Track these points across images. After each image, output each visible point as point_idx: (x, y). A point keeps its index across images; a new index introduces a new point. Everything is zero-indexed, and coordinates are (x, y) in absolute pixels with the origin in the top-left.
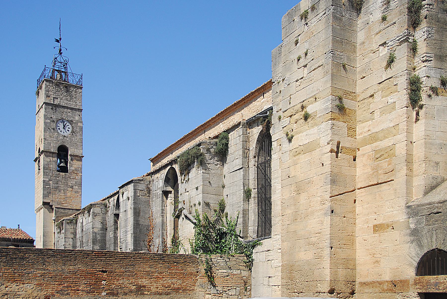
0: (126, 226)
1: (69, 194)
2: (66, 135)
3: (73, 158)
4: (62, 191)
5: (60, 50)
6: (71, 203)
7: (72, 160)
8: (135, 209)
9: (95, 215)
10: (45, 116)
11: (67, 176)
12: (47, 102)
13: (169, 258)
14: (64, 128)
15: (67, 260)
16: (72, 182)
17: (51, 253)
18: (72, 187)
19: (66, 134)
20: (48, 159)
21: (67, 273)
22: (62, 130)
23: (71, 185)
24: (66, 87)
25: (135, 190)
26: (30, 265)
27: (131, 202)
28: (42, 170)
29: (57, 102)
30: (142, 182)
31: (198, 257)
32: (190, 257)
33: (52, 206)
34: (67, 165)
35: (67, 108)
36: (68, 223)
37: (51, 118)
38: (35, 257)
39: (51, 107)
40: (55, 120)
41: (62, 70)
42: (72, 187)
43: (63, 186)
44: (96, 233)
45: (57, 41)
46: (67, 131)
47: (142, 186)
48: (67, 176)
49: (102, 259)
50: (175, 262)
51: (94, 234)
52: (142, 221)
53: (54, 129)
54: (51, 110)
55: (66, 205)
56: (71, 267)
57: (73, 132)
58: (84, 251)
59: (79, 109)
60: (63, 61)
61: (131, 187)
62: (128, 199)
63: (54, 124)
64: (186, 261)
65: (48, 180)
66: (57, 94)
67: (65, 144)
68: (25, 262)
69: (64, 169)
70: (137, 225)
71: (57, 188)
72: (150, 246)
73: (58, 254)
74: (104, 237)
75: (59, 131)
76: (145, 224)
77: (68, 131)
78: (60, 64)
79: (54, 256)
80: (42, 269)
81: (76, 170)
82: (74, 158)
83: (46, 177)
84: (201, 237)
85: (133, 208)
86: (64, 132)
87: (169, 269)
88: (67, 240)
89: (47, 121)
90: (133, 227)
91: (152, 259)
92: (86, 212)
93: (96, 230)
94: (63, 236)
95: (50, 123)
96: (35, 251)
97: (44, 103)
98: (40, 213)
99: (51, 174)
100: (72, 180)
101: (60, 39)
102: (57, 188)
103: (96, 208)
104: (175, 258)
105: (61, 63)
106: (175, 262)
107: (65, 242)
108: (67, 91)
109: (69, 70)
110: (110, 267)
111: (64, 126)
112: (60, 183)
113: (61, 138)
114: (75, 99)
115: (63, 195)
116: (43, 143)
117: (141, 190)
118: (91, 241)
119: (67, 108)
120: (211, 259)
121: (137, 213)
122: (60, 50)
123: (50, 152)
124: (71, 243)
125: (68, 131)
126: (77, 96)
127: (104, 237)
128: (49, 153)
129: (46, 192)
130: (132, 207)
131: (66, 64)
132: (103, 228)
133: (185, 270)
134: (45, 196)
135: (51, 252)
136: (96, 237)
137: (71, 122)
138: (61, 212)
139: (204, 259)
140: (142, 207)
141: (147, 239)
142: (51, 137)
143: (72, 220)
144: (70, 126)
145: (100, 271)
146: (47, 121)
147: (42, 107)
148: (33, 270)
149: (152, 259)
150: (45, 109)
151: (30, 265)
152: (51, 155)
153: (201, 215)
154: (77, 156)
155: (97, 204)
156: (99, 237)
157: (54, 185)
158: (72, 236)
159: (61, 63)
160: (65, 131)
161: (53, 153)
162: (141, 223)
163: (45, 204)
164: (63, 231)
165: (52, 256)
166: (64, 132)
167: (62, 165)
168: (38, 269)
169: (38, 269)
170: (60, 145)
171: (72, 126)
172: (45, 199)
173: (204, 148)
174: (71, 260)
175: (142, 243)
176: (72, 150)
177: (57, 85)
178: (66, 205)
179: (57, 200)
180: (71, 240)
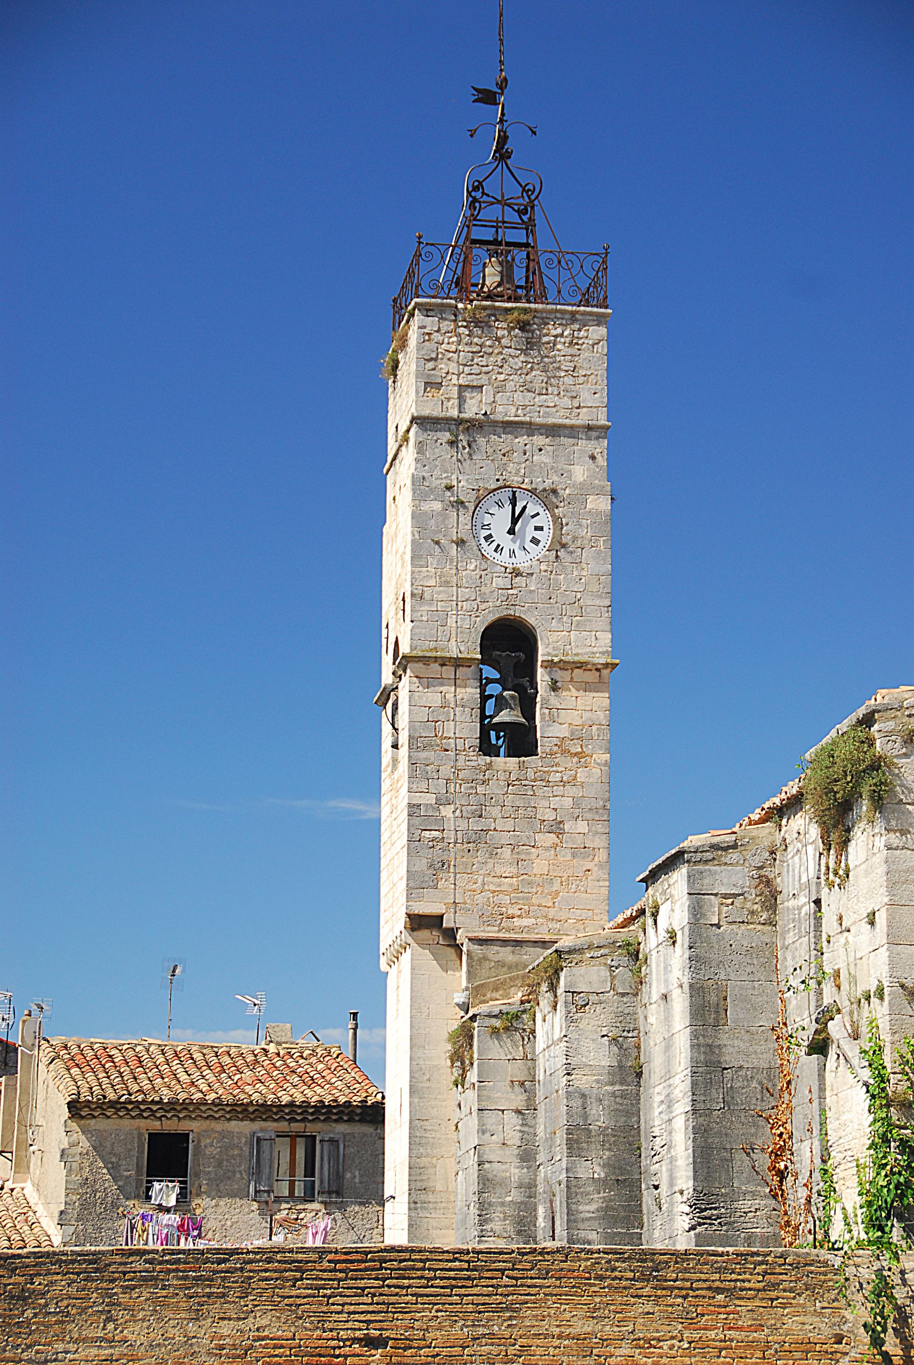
0: (668, 1076)
1: (540, 866)
2: (523, 566)
3: (562, 676)
4: (507, 851)
5: (503, 139)
6: (552, 913)
7: (554, 687)
8: (697, 990)
9: (579, 1003)
10: (418, 482)
11: (531, 774)
12: (426, 412)
13: (686, 1270)
14: (511, 531)
15: (209, 1295)
16: (555, 802)
17: (137, 1266)
18: (557, 828)
19: (522, 561)
20: (433, 697)
21: (209, 1354)
22: (505, 540)
23: (550, 816)
24: (524, 326)
25: (696, 896)
26: (48, 1326)
27: (679, 955)
28: (404, 751)
29: (473, 408)
30: (733, 856)
31: (837, 1262)
32: (796, 1266)
33: (451, 934)
34: (529, 714)
35: (530, 428)
36: (495, 1032)
37: (449, 488)
38: (72, 1290)
39: (447, 436)
40: (469, 498)
42: (557, 828)
43: (509, 825)
44: (584, 1096)
45: (487, 97)
46: (529, 546)
47: (732, 876)
48: (531, 774)
49: (362, 1283)
50: (719, 1290)
51: (576, 1103)
52: (735, 1048)
53: (461, 543)
54: (447, 452)
55: (526, 922)
56: (226, 1328)
57: (559, 545)
58: (282, 1251)
59: (589, 428)
60: (513, 191)
61: (678, 878)
62: (672, 937)
63: (465, 519)
64: (775, 1286)
66: (476, 369)
67: (518, 612)
68: (29, 1313)
69: (521, 741)
70: (709, 1069)
71: (476, 840)
72: (781, 1175)
73: (169, 1271)
74: (628, 1114)
76: (754, 1062)
77: (535, 541)
79: (149, 1280)
80: (103, 1339)
82: (567, 675)
83: (423, 786)
84: (894, 1155)
85: (686, 987)
86: (512, 553)
87: (690, 1322)
88: (491, 1119)
89: (425, 507)
90: (688, 1081)
91: (601, 1278)
92: (544, 987)
93: (583, 1081)
94: (470, 1097)
95: (443, 514)
96: (73, 1262)
97: (414, 420)
99: (446, 771)
100: (559, 790)
102: (476, 840)
103: (581, 970)
104: (719, 1270)
106: (719, 1290)
107: (482, 1131)
108: (531, 345)
109: (543, 240)
110: (402, 1321)
111: (515, 521)
112: (495, 811)
113: (499, 582)
114: (569, 380)
116: (408, 619)
117: (726, 896)
118: (561, 1137)
119: (530, 428)
120: (903, 1272)
121: (708, 1010)
123: (444, 662)
124: (514, 1139)
125: (535, 541)
126: (579, 361)
127: (628, 1114)
128: (436, 666)
129: (421, 865)
130: (686, 980)
132: (621, 1067)
133: (774, 1329)
134: (416, 884)
135: (139, 1265)
136: (585, 1116)
137: (548, 497)
138: (501, 964)
139: (867, 1274)
140: (735, 980)
141: (766, 1138)
142: (447, 584)
143: (517, 1017)
144: (544, 519)
145: (355, 1340)
146: (425, 507)
147: (406, 440)
148: (60, 1347)
149: (601, 1278)
150: (421, 447)
151: (48, 1326)
152: (448, 671)
153: (887, 1051)
154: (580, 665)
155: (590, 947)
156: (600, 1117)
157: (463, 825)
158: (518, 1100)
160: (516, 547)
161: (458, 663)
162: (730, 1057)
163: (418, 923)
164: (472, 1076)
165: (145, 1279)
167: (505, 716)
168: (84, 1340)
169: (84, 1340)
170: (491, 618)
171: (556, 519)
172: (420, 898)
173: (888, 734)
174: (224, 1295)
175: (741, 1161)
176: (554, 637)
177: (478, 323)
178: (526, 922)
179: (480, 899)
180: (511, 1119)
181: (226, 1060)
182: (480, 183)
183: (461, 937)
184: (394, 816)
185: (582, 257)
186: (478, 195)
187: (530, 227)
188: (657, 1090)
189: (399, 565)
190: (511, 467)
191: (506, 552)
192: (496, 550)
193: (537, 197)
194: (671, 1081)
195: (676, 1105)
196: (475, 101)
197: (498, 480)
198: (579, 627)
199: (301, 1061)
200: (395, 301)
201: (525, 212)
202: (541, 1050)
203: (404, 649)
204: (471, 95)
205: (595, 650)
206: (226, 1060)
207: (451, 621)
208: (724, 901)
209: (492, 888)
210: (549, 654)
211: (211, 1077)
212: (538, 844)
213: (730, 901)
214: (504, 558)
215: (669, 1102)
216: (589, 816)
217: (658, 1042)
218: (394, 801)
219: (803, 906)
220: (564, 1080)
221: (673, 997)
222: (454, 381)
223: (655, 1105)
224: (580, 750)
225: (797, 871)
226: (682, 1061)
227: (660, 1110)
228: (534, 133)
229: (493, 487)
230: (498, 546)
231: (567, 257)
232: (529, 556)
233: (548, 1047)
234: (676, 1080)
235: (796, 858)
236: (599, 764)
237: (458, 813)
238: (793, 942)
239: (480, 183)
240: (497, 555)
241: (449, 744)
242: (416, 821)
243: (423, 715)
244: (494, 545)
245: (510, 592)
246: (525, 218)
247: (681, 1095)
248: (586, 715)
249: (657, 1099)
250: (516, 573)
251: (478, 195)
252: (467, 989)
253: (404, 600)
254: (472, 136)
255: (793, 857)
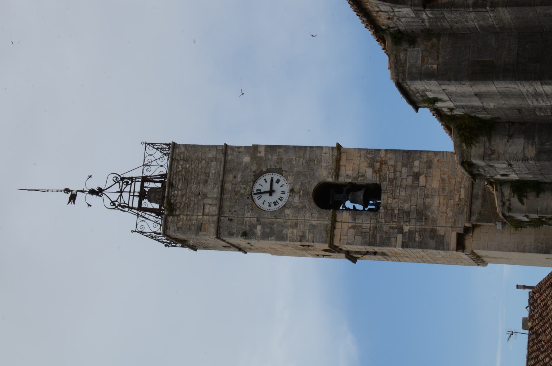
0: (521, 96)
4: (428, 200)
5: (92, 192)
16: (404, 176)
19: (286, 188)
28: (377, 249)
41: (138, 189)
42: (416, 176)
45: (73, 198)
57: (280, 171)
60: (117, 188)
65: (400, 237)
67: (311, 189)
75: (281, 204)
78: (125, 196)
81: (371, 166)
83: (393, 239)
90: (524, 82)
93: (531, 152)
98: (487, 256)
100: (398, 174)
101: (67, 190)
105: (121, 192)
109: (138, 173)
113: (296, 199)
115: (436, 198)
122: (92, 192)
129: (432, 243)
131: (123, 179)
150: (231, 235)
157: (413, 221)
159: (121, 192)
166: (283, 192)
170: (313, 204)
171: (268, 171)
172: (448, 244)
181: (535, 348)
182: (112, 202)
183: (467, 225)
184: (409, 256)
185: (146, 155)
186: (117, 204)
187: (132, 179)
188: (530, 103)
189: (287, 248)
190: (243, 191)
191: (282, 196)
192: (281, 200)
193: (119, 176)
194: (525, 94)
195: (538, 91)
196: (74, 203)
197: (248, 198)
198: (319, 162)
199: (536, 311)
200: (166, 246)
201: (127, 182)
202: (516, 176)
203: (326, 246)
204: (71, 205)
205: (331, 154)
206: (535, 348)
207: (314, 223)
208: (425, 61)
209: (445, 208)
210: (332, 177)
211: (542, 356)
212: (424, 185)
213: (426, 58)
214: (285, 197)
215: (537, 95)
216: (411, 160)
217: (504, 102)
218: (402, 255)
219: (428, 16)
220: (531, 162)
221: (478, 91)
222: (201, 217)
223: (539, 105)
224: (379, 163)
225: (409, 20)
226: (513, 87)
227: (541, 101)
228: (90, 176)
229: (251, 200)
230: (279, 199)
231: (146, 162)
232: (285, 185)
233: (514, 172)
234: (524, 90)
235: (403, 20)
236: (386, 154)
237: (407, 224)
238: (448, 22)
239: (112, 202)
240: (284, 200)
241: (373, 227)
242: (410, 244)
243: (358, 239)
244: (279, 201)
245: (301, 194)
246: (130, 182)
247: (532, 88)
248: (362, 159)
249: (535, 103)
250: (292, 191)
251: (117, 204)
252: (495, 222)
253: (304, 246)
254: (90, 206)
255: (402, 22)
